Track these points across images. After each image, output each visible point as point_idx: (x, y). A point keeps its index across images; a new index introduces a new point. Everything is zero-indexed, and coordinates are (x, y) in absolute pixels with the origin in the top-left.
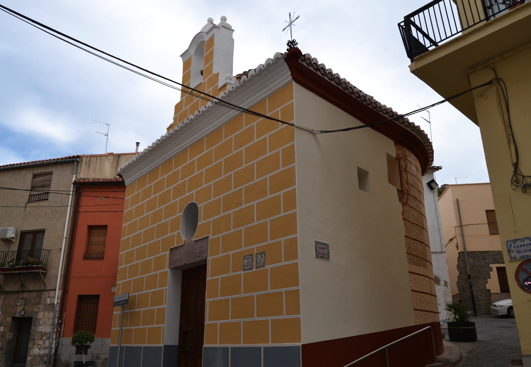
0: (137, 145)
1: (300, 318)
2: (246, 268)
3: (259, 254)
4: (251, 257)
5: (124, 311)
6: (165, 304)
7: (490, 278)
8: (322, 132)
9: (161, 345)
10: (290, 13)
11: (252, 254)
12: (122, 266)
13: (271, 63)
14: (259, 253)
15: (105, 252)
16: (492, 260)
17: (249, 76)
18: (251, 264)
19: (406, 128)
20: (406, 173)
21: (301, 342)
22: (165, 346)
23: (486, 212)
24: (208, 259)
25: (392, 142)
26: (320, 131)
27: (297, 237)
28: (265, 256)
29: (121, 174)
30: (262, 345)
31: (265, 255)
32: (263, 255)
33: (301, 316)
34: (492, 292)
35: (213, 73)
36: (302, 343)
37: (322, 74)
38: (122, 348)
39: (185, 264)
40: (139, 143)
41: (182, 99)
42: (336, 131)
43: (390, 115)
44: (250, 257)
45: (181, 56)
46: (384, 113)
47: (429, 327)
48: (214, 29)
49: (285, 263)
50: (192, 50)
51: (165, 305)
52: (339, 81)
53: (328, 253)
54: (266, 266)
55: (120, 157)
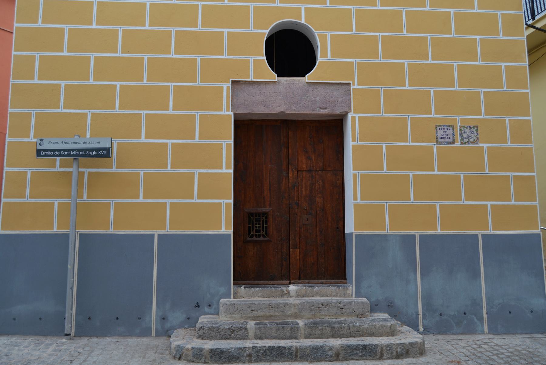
2: (440, 140)
3: (467, 128)
5: (75, 230)
14: (466, 126)
18: (451, 137)
28: (477, 132)
30: (480, 233)
31: (477, 131)
54: (480, 144)
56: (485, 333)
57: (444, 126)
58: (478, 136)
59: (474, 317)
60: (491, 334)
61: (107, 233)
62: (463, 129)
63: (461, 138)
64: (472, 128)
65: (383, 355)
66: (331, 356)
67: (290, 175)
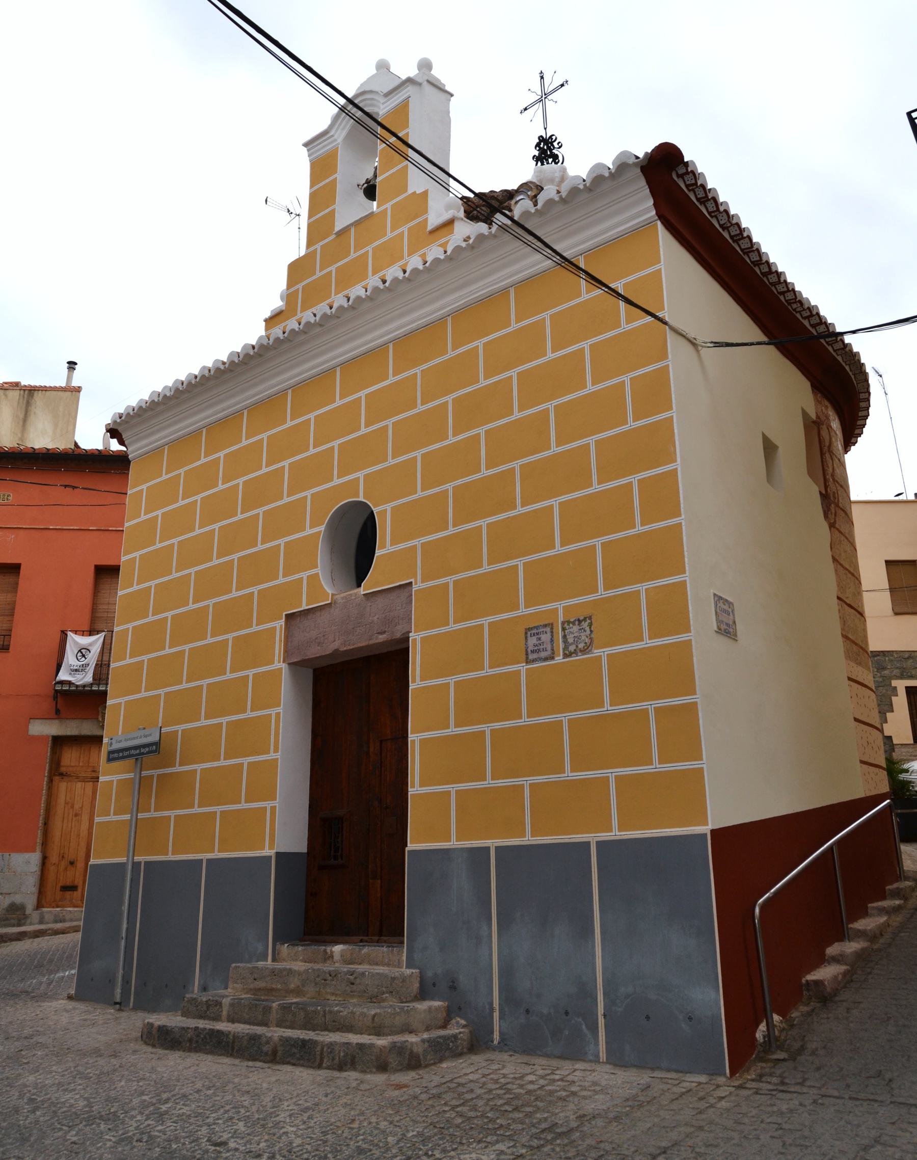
0: (69, 368)
1: (703, 768)
2: (531, 657)
3: (573, 623)
4: (548, 629)
5: (141, 771)
6: (276, 751)
7: (893, 711)
8: (718, 345)
9: (268, 852)
10: (541, 72)
11: (552, 624)
12: (125, 659)
13: (607, 174)
15: (13, 632)
16: (896, 672)
17: (540, 205)
18: (549, 648)
19: (834, 354)
20: (831, 456)
21: (708, 825)
22: (277, 854)
23: (886, 565)
24: (410, 638)
25: (806, 385)
26: (712, 342)
27: (685, 581)
28: (590, 628)
29: (120, 429)
30: (593, 837)
31: (590, 625)
32: (585, 625)
33: (704, 764)
34: (895, 742)
35: (410, 191)
36: (710, 827)
37: (710, 213)
38: (136, 865)
39: (337, 650)
40: (75, 364)
41: (312, 249)
42: (752, 344)
43: (812, 323)
44: (544, 630)
45: (306, 145)
46: (804, 316)
47: (888, 801)
48: (408, 86)
49: (650, 642)
50: (338, 132)
51: (275, 752)
52: (738, 232)
53: (734, 622)
54: (596, 651)
55: (33, 393)
56: (601, 1060)
57: (537, 627)
58: (592, 636)
59: (583, 1022)
60: (610, 1064)
61: (262, 855)
62: (567, 627)
63: (563, 646)
64: (583, 620)
65: (323, 1061)
66: (266, 1054)
67: (371, 750)
